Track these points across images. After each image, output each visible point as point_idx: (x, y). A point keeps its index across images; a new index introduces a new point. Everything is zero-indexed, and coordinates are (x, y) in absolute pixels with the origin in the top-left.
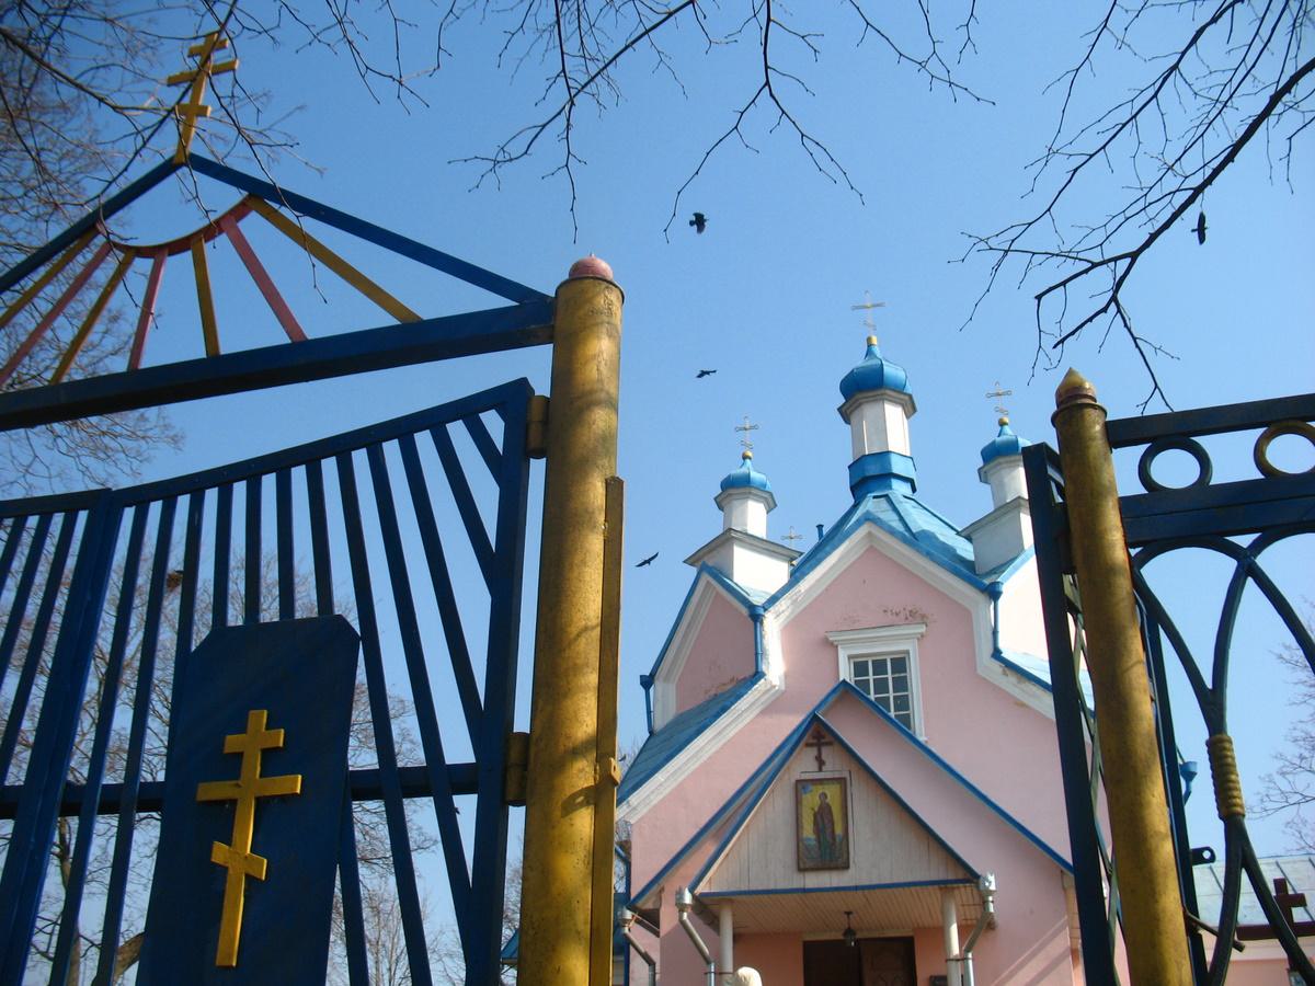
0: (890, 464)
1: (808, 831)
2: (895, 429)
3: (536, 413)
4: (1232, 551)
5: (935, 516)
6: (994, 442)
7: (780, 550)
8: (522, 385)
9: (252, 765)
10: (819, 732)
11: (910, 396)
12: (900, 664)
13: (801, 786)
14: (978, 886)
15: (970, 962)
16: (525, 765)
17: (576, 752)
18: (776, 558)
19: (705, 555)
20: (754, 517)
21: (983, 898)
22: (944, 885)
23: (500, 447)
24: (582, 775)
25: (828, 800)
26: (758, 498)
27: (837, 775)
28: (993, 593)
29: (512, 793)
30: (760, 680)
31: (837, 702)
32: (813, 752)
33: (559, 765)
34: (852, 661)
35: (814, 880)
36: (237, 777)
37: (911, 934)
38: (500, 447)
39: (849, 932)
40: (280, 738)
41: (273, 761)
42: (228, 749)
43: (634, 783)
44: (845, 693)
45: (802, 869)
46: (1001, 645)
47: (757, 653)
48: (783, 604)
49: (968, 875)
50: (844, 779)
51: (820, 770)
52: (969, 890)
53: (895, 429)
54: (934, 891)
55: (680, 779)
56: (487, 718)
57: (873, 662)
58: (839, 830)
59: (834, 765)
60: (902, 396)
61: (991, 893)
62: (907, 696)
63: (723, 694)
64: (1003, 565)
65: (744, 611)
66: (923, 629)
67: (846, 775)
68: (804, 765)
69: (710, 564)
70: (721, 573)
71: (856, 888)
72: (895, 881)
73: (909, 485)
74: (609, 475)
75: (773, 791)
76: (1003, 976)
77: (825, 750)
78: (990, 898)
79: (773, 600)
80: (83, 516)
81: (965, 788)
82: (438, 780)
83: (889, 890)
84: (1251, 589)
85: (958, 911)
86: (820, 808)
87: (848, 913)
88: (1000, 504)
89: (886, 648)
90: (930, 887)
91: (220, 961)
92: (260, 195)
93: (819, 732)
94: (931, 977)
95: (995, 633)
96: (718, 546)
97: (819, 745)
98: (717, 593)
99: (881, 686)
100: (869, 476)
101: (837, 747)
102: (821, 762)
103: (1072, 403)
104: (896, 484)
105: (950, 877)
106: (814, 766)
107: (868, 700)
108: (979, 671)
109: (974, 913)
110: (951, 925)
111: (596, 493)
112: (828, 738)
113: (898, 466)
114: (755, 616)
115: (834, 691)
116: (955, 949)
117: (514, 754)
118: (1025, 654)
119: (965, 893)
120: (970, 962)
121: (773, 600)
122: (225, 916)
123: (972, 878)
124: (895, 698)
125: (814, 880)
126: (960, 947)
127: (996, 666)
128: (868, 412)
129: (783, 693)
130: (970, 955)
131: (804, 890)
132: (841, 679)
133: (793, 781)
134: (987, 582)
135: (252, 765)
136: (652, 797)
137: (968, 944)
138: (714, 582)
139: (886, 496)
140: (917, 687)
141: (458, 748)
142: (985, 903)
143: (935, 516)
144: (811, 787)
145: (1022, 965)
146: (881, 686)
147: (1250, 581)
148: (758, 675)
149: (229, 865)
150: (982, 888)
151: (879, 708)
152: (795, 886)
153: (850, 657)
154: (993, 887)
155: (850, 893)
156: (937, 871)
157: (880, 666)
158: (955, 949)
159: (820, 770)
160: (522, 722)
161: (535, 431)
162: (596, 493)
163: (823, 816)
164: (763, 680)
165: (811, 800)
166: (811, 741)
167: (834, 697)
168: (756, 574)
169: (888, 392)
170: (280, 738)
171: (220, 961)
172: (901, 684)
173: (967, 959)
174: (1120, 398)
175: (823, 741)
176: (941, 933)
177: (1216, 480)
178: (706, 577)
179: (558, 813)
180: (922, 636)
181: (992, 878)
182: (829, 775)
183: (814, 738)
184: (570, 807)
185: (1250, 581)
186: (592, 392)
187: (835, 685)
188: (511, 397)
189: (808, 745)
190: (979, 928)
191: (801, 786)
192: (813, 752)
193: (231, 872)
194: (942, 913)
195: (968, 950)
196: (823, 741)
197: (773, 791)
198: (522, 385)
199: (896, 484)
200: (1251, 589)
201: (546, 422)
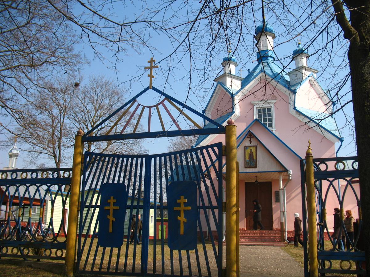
0: (268, 54)
1: (247, 159)
2: (269, 43)
3: (223, 148)
4: (329, 181)
5: (280, 68)
6: (296, 50)
7: (238, 78)
8: (221, 143)
9: (182, 205)
10: (250, 134)
11: (274, 34)
12: (270, 110)
13: (246, 147)
14: (288, 173)
15: (285, 190)
16: (225, 207)
17: (233, 206)
18: (237, 80)
19: (219, 79)
20: (233, 69)
21: (289, 175)
22: (280, 172)
23: (218, 154)
24: (234, 209)
25: (252, 151)
26: (233, 64)
27: (255, 145)
28: (294, 92)
29: (224, 210)
30: (233, 114)
31: (253, 124)
32: (249, 139)
33: (231, 208)
34: (257, 109)
35: (248, 170)
36: (180, 207)
37: (270, 181)
38: (218, 154)
39: (256, 181)
40: (186, 201)
41: (186, 204)
42: (178, 202)
43: (201, 140)
44: (256, 122)
45: (245, 167)
46: (296, 106)
47: (233, 106)
48: (240, 94)
49: (285, 170)
50: (256, 146)
51: (250, 143)
52: (285, 173)
53: (269, 43)
54: (277, 173)
55: (213, 139)
56: (219, 199)
57: (263, 109)
58: (255, 158)
59: (254, 143)
60: (272, 34)
61: (290, 174)
62: (271, 118)
63: (223, 116)
64: (297, 84)
65: (230, 95)
66: (276, 101)
67: (257, 145)
68: (247, 142)
69: (220, 81)
70: (223, 84)
71: (259, 172)
72: (268, 171)
73: (273, 59)
74: (236, 161)
75: (239, 149)
76: (293, 191)
77: (252, 139)
78: (290, 176)
79: (237, 93)
80: (144, 159)
81: (285, 146)
82: (212, 207)
83: (266, 173)
84: (331, 187)
85: (282, 177)
86: (251, 153)
87: (256, 177)
88: (297, 67)
89: (266, 105)
90: (276, 172)
91: (181, 234)
92: (168, 98)
93: (250, 134)
94: (275, 191)
95: (294, 103)
96: (222, 77)
97: (250, 138)
98: (222, 89)
99: (265, 120)
100: (262, 57)
101: (255, 138)
102: (251, 142)
103: (308, 154)
104: (269, 58)
105: (281, 170)
106: (249, 142)
107: (262, 123)
108: (290, 112)
109: (286, 177)
110: (281, 181)
111: (234, 165)
112: (252, 136)
113: (270, 53)
114: (232, 97)
115: (253, 121)
116: (282, 187)
117: (224, 205)
118: (302, 108)
119: (284, 173)
120: (285, 190)
121: (237, 93)
122: (181, 227)
123: (286, 170)
124: (268, 118)
125: (248, 170)
126: (283, 186)
127: (295, 111)
128: (263, 38)
129: (240, 117)
130: (285, 188)
131: (246, 172)
132: (255, 118)
133: (244, 146)
134: (293, 88)
135: (182, 205)
136: (206, 143)
137: (285, 186)
138: (221, 86)
139: (267, 62)
140: (274, 118)
141: (215, 203)
142: (289, 176)
143: (280, 68)
144: (248, 148)
145: (295, 191)
146: (265, 120)
147: (331, 186)
148: (233, 112)
149: (181, 220)
150: (289, 173)
151: (264, 126)
152: (244, 171)
153: (257, 108)
154: (291, 173)
155: (257, 173)
156: (278, 169)
157: (264, 110)
158: (282, 187)
159: (250, 143)
160: (224, 200)
161: (223, 152)
162: (234, 165)
163: (251, 155)
164: (234, 114)
165: (248, 151)
166: (248, 136)
167: (254, 122)
168: (234, 85)
169: (268, 33)
170: (186, 201)
171: (181, 234)
172: (270, 115)
173: (284, 189)
174: (315, 155)
175: (251, 136)
176: (278, 181)
177: (328, 170)
178: (219, 85)
179: (231, 215)
180: (276, 103)
181: (291, 171)
182: (253, 145)
183: (249, 136)
184: (233, 214)
185: (331, 186)
186: (233, 147)
187: (253, 121)
188: (219, 145)
189: (248, 137)
190: (287, 181)
191: (246, 147)
192: (249, 139)
193: (181, 221)
194: (279, 177)
195: (284, 187)
196: (251, 136)
197: (239, 149)
198: (221, 143)
199: (269, 58)
200: (331, 187)
201: (225, 150)
